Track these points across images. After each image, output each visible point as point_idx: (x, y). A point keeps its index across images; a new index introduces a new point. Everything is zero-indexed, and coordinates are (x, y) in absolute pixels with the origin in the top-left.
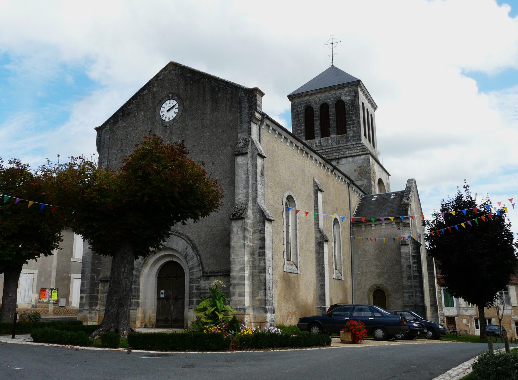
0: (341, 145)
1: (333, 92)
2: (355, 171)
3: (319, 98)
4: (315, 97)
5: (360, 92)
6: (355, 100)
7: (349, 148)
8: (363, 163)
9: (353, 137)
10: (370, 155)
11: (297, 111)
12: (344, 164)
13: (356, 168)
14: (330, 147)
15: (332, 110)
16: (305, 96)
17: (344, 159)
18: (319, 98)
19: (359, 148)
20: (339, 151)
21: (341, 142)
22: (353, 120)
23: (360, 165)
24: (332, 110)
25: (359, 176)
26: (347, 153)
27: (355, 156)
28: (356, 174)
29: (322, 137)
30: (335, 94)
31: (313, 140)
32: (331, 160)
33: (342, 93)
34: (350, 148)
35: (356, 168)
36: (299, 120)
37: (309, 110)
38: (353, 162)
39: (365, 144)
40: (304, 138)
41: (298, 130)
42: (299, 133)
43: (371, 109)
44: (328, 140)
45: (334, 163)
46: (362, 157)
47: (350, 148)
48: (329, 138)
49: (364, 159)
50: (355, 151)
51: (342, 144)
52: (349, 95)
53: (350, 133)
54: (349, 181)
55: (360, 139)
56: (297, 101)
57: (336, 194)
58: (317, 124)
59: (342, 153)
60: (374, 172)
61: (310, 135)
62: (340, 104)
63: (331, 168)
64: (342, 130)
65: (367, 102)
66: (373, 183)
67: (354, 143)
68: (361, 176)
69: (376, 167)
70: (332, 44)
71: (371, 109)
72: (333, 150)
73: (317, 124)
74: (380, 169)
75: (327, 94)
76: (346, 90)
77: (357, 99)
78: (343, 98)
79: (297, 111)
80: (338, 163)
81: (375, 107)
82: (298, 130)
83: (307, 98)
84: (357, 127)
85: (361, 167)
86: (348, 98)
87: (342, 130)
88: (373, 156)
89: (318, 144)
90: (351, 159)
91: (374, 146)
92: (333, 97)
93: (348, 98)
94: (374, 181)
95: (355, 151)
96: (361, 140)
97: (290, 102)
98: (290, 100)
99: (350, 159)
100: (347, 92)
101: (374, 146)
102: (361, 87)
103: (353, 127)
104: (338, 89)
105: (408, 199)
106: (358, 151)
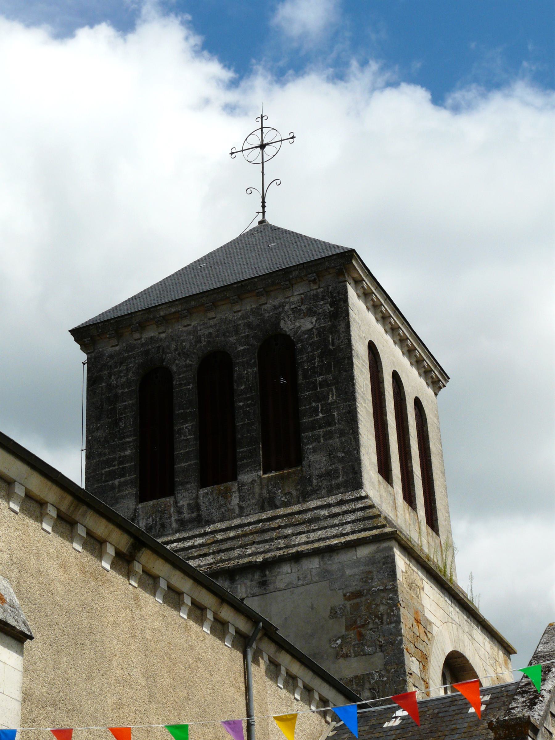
0: (282, 511)
1: (249, 305)
2: (334, 614)
3: (195, 330)
4: (179, 328)
5: (352, 293)
6: (333, 330)
7: (310, 521)
8: (367, 578)
9: (329, 475)
10: (394, 544)
11: (110, 387)
12: (290, 586)
13: (338, 600)
14: (237, 522)
15: (246, 373)
16: (142, 327)
17: (286, 568)
18: (195, 330)
19: (351, 517)
20: (267, 536)
21: (281, 498)
22: (328, 409)
23: (355, 585)
24: (246, 373)
25: (352, 634)
26: (301, 542)
27: (331, 550)
28: (339, 627)
29: (203, 485)
30: (255, 312)
31: (170, 500)
32: (232, 574)
33: (282, 305)
34: (317, 519)
35: (338, 600)
36: (116, 423)
37: (154, 381)
38: (325, 574)
39: (386, 509)
40: (133, 491)
41: (109, 463)
42: (112, 475)
43: (415, 384)
44: (226, 494)
45: (242, 589)
46: (363, 552)
47: (317, 519)
48: (234, 486)
49: (371, 561)
50: (334, 531)
51: (286, 505)
52: (311, 313)
53: (316, 461)
54: (243, 625)
55: (355, 481)
56: (109, 348)
57: (151, 676)
58: (186, 432)
59: (282, 543)
60: (420, 620)
61: (155, 482)
62: (277, 349)
63: (118, 540)
64: (284, 451)
65: (388, 339)
66: (413, 665)
67: (332, 500)
68: (361, 636)
69: (430, 599)
70: (262, 146)
71: (415, 384)
72: (245, 535)
73: (186, 432)
74: (455, 612)
75: (225, 313)
76: (298, 292)
77: (342, 326)
78: (287, 326)
79: (110, 387)
80: (263, 584)
81: (436, 378)
82: (109, 463)
83: (151, 333)
84: (342, 433)
85: (357, 594)
86: (307, 324)
87: (284, 451)
88: (410, 552)
89: (186, 515)
90: (314, 564)
91: (432, 521)
92: (249, 326)
93: (307, 324)
94: (424, 660)
95: (334, 531)
96: (359, 485)
97: (84, 357)
98: (84, 348)
99: (313, 565)
100: (302, 301)
101: (432, 521)
102: (358, 282)
103: (328, 435)
104: (267, 293)
105: (532, 704)
106: (348, 528)
